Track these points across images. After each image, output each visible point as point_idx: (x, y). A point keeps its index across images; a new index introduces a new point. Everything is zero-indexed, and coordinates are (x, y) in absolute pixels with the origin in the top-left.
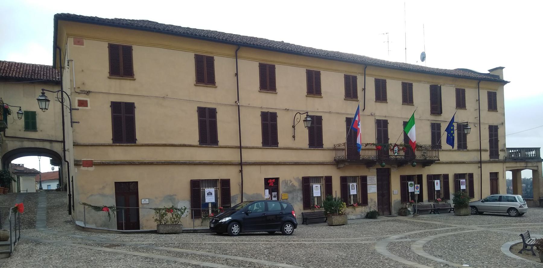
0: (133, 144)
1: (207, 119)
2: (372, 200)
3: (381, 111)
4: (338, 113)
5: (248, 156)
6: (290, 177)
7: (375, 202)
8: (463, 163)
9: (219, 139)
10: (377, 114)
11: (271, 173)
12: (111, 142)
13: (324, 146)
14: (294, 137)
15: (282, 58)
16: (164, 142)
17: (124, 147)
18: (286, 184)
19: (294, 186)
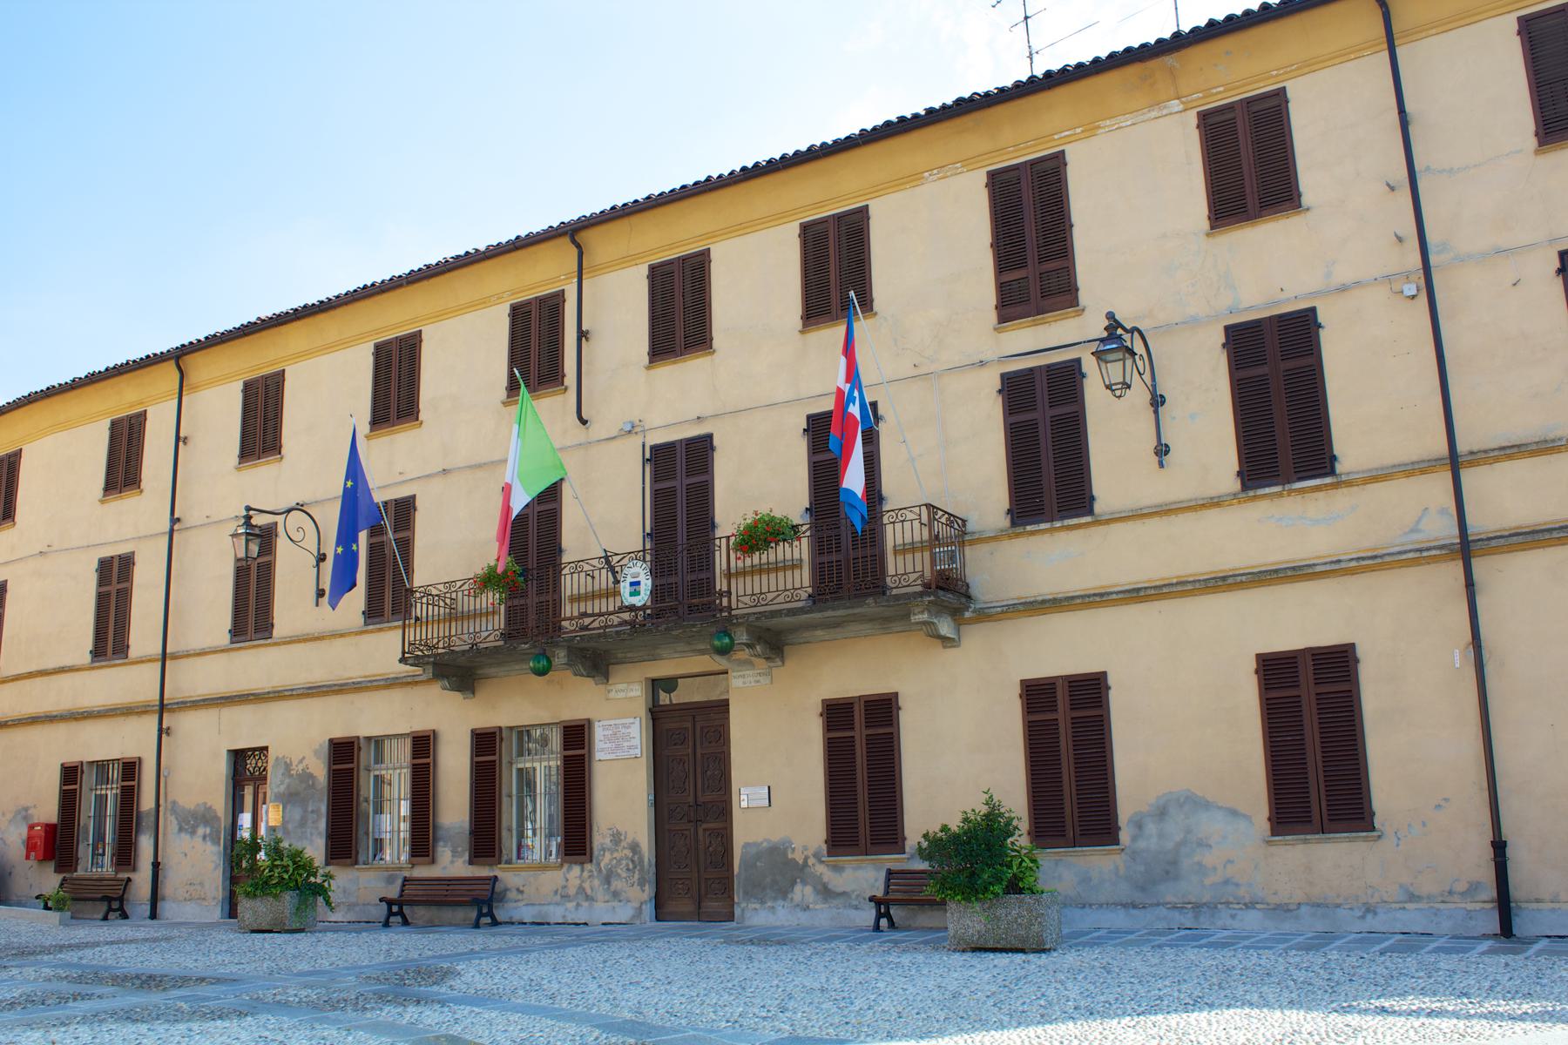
0: (1328, 480)
1: (1043, 415)
2: (617, 838)
3: (675, 400)
4: (479, 466)
5: (190, 680)
6: (297, 740)
7: (635, 848)
8: (1136, 595)
9: (1339, 447)
10: (654, 419)
11: (245, 729)
12: (1234, 485)
13: (1098, 507)
14: (1162, 450)
15: (295, 336)
16: (33, 668)
17: (1081, 532)
18: (288, 766)
19: (311, 776)
